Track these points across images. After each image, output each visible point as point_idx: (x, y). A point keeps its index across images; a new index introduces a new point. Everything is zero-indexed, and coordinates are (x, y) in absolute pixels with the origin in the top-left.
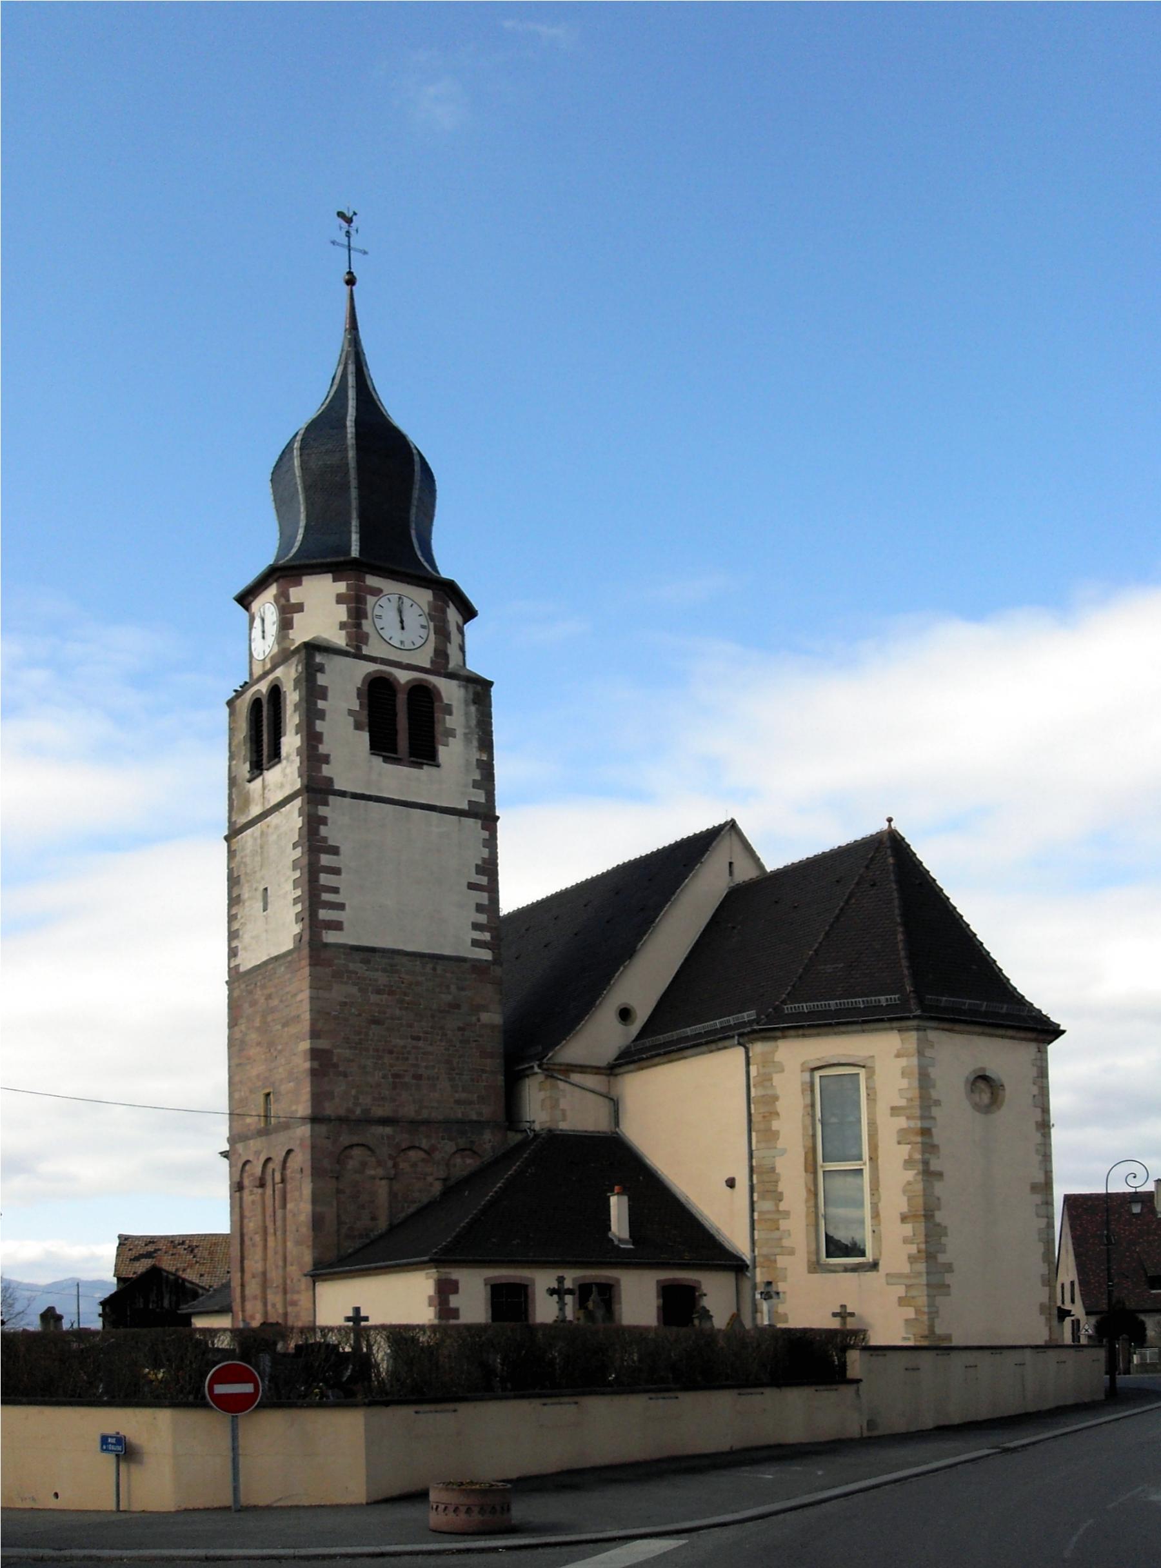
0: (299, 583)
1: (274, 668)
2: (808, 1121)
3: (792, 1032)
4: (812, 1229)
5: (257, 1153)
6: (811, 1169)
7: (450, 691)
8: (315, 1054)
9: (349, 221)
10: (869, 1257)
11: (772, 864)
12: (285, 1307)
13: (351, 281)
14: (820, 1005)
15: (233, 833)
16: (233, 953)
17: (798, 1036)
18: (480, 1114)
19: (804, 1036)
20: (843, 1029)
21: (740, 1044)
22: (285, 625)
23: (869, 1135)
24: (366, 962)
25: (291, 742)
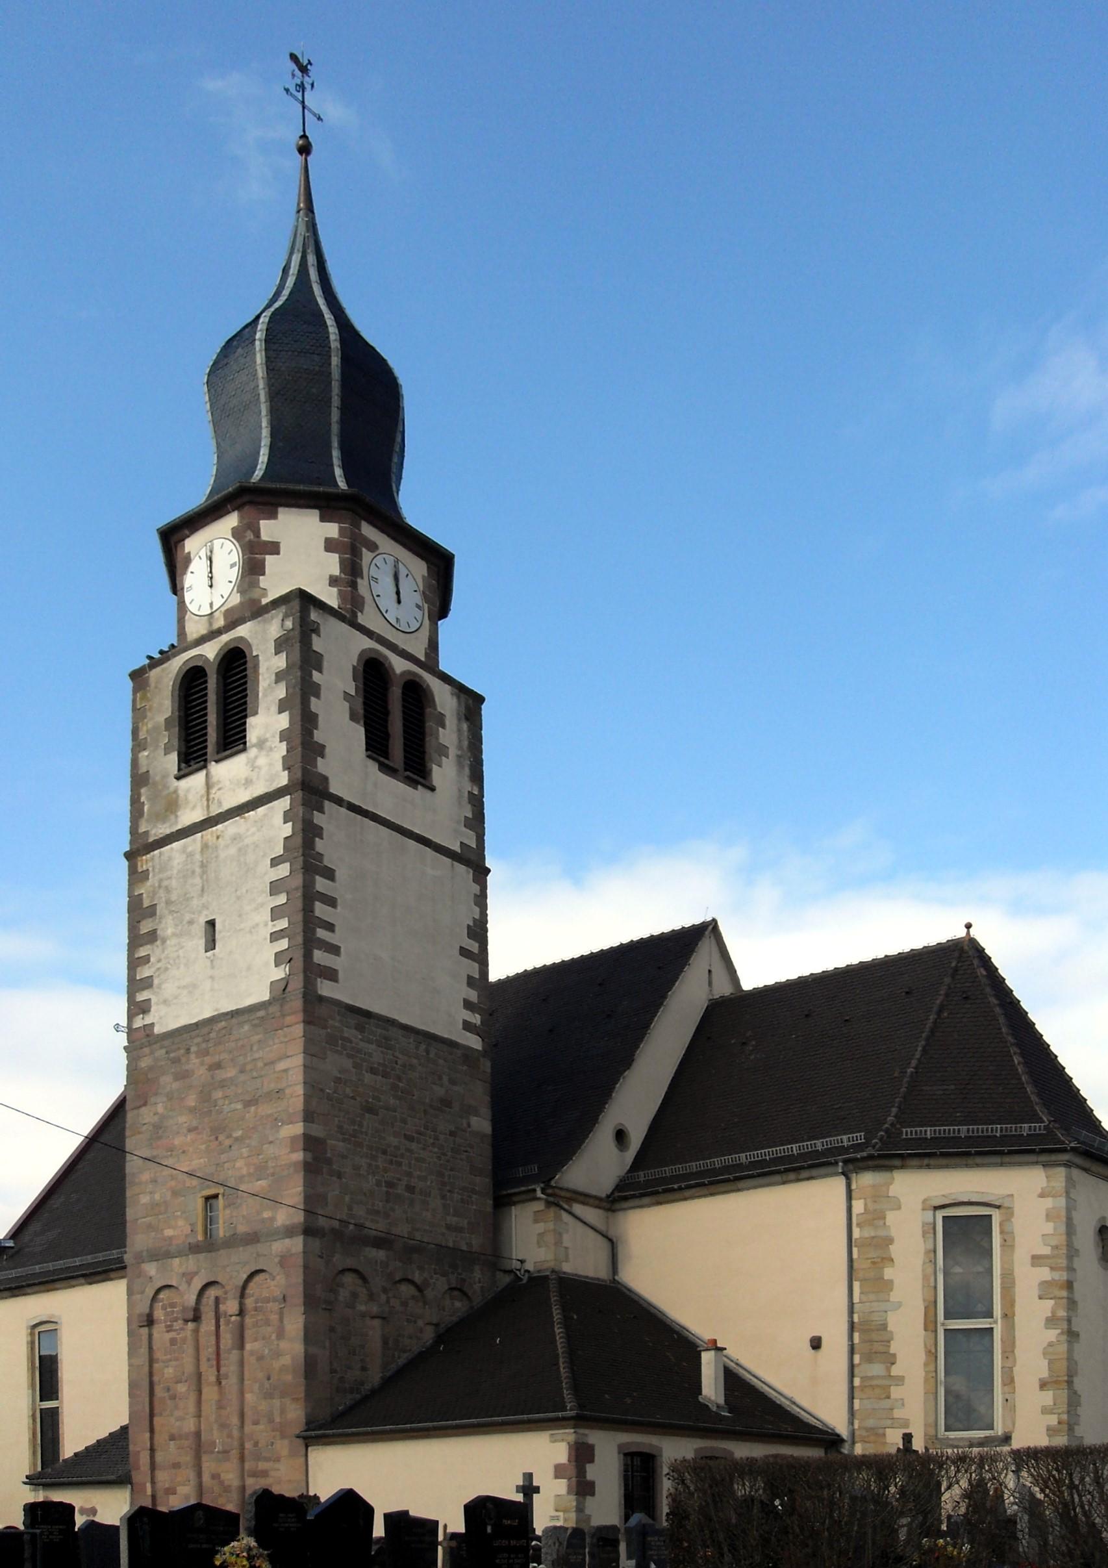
0: (273, 516)
1: (231, 625)
2: (930, 1270)
3: (915, 1162)
4: (931, 1397)
5: (189, 1277)
6: (931, 1327)
7: (444, 700)
8: (310, 1143)
9: (304, 70)
10: (999, 1430)
11: (747, 984)
12: (242, 1478)
13: (305, 149)
14: (779, 1150)
15: (140, 848)
16: (137, 1008)
17: (920, 1167)
18: (469, 1245)
19: (928, 1166)
20: (979, 1160)
21: (843, 1173)
22: (252, 568)
23: (1003, 1288)
24: (360, 1028)
25: (267, 723)
